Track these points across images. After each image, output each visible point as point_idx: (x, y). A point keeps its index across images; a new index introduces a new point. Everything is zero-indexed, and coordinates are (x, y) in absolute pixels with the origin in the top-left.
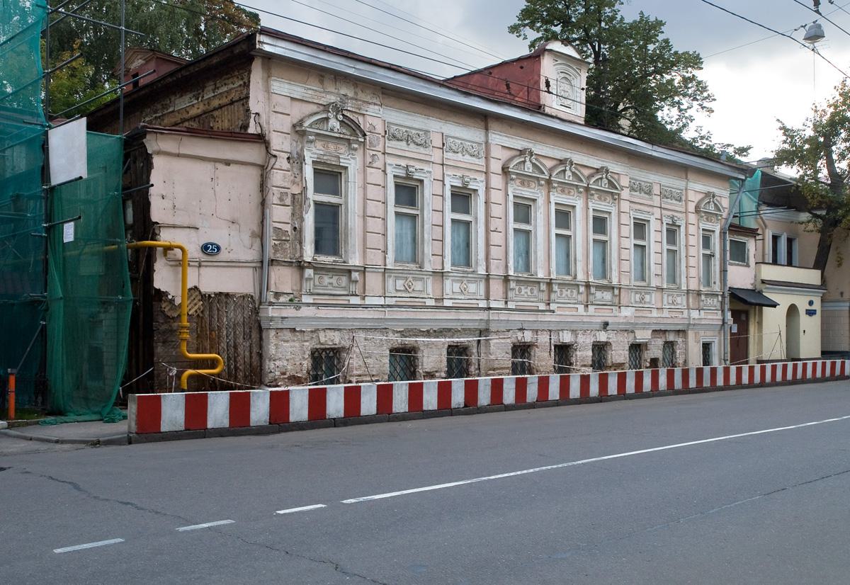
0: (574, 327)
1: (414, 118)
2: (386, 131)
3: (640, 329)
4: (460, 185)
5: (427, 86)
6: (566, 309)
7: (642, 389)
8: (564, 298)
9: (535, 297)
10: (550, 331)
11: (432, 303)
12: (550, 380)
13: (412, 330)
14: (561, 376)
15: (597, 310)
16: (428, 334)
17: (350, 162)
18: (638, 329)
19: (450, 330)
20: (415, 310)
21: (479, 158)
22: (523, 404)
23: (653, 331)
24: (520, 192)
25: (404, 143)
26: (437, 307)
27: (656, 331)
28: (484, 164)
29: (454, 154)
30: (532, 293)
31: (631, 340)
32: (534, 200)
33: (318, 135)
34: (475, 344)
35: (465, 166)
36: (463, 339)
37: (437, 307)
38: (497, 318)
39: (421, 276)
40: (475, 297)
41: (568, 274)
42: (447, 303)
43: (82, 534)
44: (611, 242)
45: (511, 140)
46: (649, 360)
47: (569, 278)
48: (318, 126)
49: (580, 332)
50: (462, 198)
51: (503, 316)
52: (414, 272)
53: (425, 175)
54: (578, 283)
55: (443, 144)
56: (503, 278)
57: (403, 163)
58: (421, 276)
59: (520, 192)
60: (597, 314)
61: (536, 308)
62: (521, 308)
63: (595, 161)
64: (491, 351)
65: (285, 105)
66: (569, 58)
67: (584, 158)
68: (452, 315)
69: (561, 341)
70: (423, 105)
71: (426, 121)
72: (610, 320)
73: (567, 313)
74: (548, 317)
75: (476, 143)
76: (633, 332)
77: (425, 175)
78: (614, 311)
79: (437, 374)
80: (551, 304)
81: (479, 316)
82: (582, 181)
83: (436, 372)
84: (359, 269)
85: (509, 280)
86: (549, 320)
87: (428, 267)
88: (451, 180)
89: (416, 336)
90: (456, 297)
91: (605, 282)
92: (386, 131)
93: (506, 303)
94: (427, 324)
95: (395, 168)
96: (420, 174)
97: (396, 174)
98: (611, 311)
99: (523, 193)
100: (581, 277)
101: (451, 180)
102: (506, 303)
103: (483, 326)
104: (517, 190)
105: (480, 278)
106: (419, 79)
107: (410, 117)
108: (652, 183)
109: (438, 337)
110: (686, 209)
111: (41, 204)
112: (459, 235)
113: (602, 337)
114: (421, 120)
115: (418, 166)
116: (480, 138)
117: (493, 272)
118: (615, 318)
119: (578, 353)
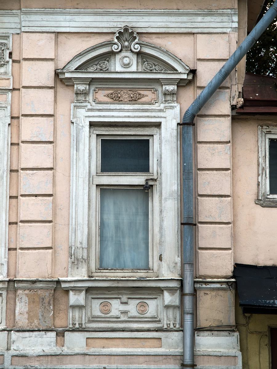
32: (158, 125)
65: (43, 46)
85: (67, 291)
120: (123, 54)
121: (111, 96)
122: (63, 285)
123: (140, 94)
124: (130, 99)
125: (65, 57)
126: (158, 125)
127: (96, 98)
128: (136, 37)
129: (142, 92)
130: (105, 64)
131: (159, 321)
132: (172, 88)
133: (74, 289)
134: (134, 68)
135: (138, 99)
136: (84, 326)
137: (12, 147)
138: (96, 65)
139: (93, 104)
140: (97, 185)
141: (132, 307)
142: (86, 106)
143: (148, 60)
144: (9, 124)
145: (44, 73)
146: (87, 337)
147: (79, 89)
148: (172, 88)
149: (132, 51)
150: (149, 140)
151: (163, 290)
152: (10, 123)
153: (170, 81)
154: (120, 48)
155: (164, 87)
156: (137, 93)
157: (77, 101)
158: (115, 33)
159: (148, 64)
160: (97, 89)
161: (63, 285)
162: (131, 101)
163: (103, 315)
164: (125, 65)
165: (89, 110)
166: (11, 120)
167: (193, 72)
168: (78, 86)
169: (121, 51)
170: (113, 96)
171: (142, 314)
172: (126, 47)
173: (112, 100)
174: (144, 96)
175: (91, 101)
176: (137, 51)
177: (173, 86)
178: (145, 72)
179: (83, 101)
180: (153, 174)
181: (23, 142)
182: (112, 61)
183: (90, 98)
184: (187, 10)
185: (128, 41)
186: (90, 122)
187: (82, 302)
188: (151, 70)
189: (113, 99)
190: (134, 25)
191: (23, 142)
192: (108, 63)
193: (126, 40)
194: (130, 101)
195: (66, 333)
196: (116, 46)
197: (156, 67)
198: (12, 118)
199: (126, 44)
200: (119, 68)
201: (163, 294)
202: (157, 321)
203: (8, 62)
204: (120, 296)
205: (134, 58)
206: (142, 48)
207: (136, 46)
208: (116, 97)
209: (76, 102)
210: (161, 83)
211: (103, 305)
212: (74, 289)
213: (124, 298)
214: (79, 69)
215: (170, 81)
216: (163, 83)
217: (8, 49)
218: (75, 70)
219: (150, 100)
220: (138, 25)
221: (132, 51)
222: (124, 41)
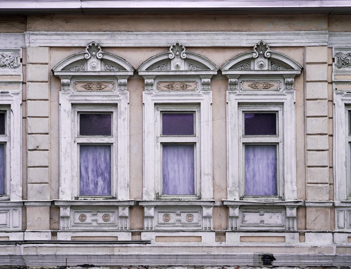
6: (175, 239)
9: (113, 225)
21: (15, 68)
24: (84, 98)
30: (105, 220)
32: (116, 105)
33: (73, 77)
38: (35, 254)
41: (193, 193)
44: (283, 145)
47: (191, 198)
59: (84, 98)
61: (114, 239)
62: (80, 239)
63: (245, 37)
65: (43, 56)
67: (216, 37)
72: (275, 253)
78: (287, 240)
80: (142, 234)
82: (208, 69)
84: (327, 205)
85: (58, 208)
86: (137, 253)
88: (344, 98)
91: (276, 200)
95: (346, 95)
98: (282, 239)
101: (344, 98)
102: (54, 234)
105: (16, 206)
110: (25, 76)
112: (268, 159)
117: (32, 197)
118: (289, 250)
120: (259, 59)
121: (86, 86)
122: (56, 204)
124: (264, 88)
125: (53, 63)
126: (116, 105)
127: (159, 88)
128: (268, 48)
129: (271, 83)
130: (164, 67)
131: (200, 226)
132: (208, 80)
134: (98, 69)
135: (269, 88)
136: (238, 229)
137: (332, 117)
138: (241, 67)
139: (157, 91)
140: (243, 143)
141: (183, 217)
142: (236, 92)
143: (108, 64)
145: (43, 73)
146: (156, 236)
147: (288, 81)
148: (208, 80)
150: (4, 113)
151: (144, 207)
152: (212, 103)
153: (206, 76)
154: (257, 56)
156: (184, 84)
157: (230, 89)
158: (86, 47)
159: (108, 66)
160: (77, 82)
161: (56, 204)
162: (264, 89)
164: (94, 66)
166: (22, 102)
167: (303, 70)
168: (287, 79)
169: (257, 58)
170: (253, 86)
171: (166, 221)
172: (261, 55)
173: (85, 89)
175: (239, 89)
178: (272, 70)
179: (207, 89)
180: (196, 135)
183: (154, 87)
185: (262, 51)
186: (238, 103)
188: (110, 70)
189: (86, 88)
190: (267, 41)
192: (249, 66)
194: (263, 89)
195: (306, 233)
197: (280, 68)
198: (23, 101)
200: (256, 68)
201: (118, 209)
202: (282, 226)
203: (20, 65)
204: (259, 211)
205: (266, 61)
206: (272, 55)
207: (268, 54)
208: (255, 87)
209: (229, 89)
210: (117, 78)
213: (178, 212)
214: (148, 70)
215: (206, 76)
216: (285, 77)
218: (146, 70)
219: (276, 88)
221: (265, 58)
222: (93, 52)
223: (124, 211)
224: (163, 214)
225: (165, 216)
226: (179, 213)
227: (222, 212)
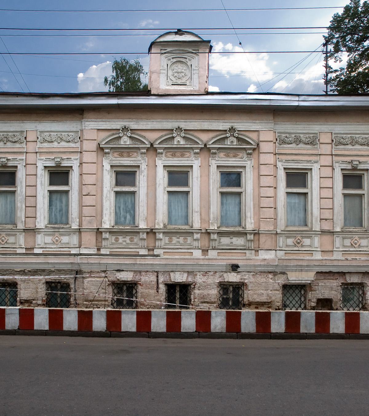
0: (190, 269)
1: (11, 125)
2: (277, 139)
3: (292, 271)
4: (54, 165)
5: (5, 98)
7: (180, 329)
8: (175, 244)
9: (136, 244)
10: (157, 272)
11: (24, 251)
12: (35, 312)
13: (7, 270)
14: (316, 313)
15: (287, 255)
16: (23, 272)
17: (193, 162)
18: (289, 271)
19: (44, 271)
20: (5, 256)
22: (4, 330)
23: (317, 273)
24: (118, 162)
25: (293, 145)
26: (26, 254)
27: (322, 272)
28: (79, 146)
29: (74, 144)
30: (131, 241)
31: (281, 280)
32: (139, 167)
34: (73, 281)
35: (58, 151)
36: (63, 277)
37: (26, 254)
38: (86, 262)
39: (14, 233)
40: (67, 246)
41: (187, 224)
42: (36, 251)
43: (102, 378)
44: (245, 193)
45: (107, 123)
46: (315, 300)
47: (187, 227)
48: (167, 143)
49: (198, 274)
50: (59, 175)
51: (94, 260)
52: (6, 230)
53: (18, 162)
54: (193, 231)
55: (333, 141)
56: (96, 230)
57: (349, 159)
58: (14, 233)
59: (118, 162)
60: (220, 257)
61: (137, 253)
62: (118, 253)
64: (85, 287)
66: (176, 43)
68: (41, 260)
69: (172, 280)
70: (20, 114)
71: (22, 125)
72: (240, 263)
73: (177, 257)
74: (149, 261)
75: (17, 132)
76: (284, 273)
77: (18, 162)
78: (248, 255)
79: (34, 302)
81: (70, 260)
82: (198, 143)
83: (34, 300)
85: (101, 233)
86: (151, 263)
87: (21, 226)
89: (14, 274)
90: (48, 246)
92: (277, 139)
93: (99, 250)
94: (19, 266)
95: (341, 164)
96: (13, 162)
97: (285, 167)
98: (244, 255)
99: (121, 162)
100: (197, 225)
102: (99, 250)
103: (76, 268)
104: (114, 160)
106: (164, 97)
107: (6, 125)
108: (317, 134)
109: (34, 276)
110: (81, 148)
111: (153, 210)
113: (233, 278)
114: (16, 124)
115: (10, 157)
116: (77, 127)
119: (197, 291)
122: (100, 230)
123: (237, 154)
131: (192, 245)
133: (213, 233)
144: (200, 166)
145: (93, 146)
149: (127, 136)
154: (229, 136)
155: (194, 150)
163: (131, 243)
164: (125, 141)
165: (217, 161)
172: (232, 135)
174: (239, 155)
176: (183, 136)
177: (198, 150)
181: (83, 174)
182: (120, 140)
184: (222, 120)
187: (145, 237)
189: (120, 156)
191: (83, 174)
193: (179, 132)
195: (259, 251)
196: (228, 134)
199: (232, 133)
201: (139, 234)
202: (191, 245)
205: (235, 139)
207: (129, 134)
211: (169, 239)
212: (213, 233)
215: (197, 148)
217: (318, 138)
220: (238, 127)
223: (143, 236)
224: (168, 237)
225: (169, 239)
226: (178, 237)
227: (206, 236)
